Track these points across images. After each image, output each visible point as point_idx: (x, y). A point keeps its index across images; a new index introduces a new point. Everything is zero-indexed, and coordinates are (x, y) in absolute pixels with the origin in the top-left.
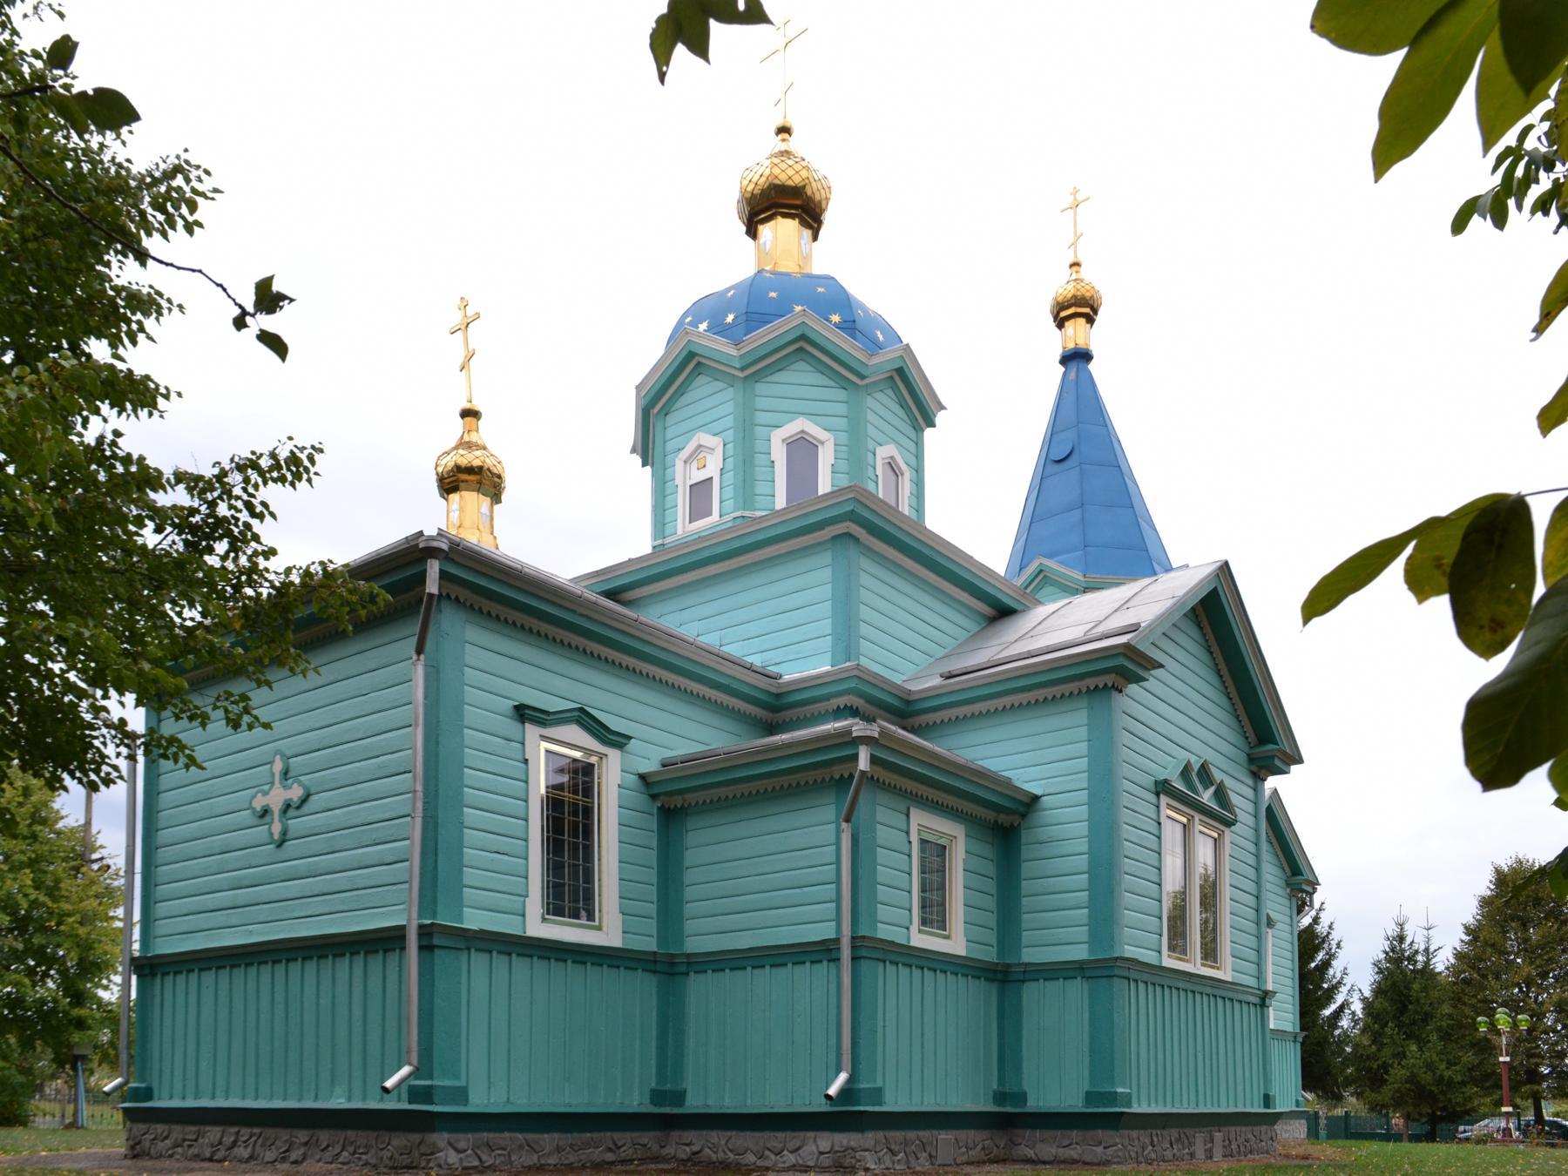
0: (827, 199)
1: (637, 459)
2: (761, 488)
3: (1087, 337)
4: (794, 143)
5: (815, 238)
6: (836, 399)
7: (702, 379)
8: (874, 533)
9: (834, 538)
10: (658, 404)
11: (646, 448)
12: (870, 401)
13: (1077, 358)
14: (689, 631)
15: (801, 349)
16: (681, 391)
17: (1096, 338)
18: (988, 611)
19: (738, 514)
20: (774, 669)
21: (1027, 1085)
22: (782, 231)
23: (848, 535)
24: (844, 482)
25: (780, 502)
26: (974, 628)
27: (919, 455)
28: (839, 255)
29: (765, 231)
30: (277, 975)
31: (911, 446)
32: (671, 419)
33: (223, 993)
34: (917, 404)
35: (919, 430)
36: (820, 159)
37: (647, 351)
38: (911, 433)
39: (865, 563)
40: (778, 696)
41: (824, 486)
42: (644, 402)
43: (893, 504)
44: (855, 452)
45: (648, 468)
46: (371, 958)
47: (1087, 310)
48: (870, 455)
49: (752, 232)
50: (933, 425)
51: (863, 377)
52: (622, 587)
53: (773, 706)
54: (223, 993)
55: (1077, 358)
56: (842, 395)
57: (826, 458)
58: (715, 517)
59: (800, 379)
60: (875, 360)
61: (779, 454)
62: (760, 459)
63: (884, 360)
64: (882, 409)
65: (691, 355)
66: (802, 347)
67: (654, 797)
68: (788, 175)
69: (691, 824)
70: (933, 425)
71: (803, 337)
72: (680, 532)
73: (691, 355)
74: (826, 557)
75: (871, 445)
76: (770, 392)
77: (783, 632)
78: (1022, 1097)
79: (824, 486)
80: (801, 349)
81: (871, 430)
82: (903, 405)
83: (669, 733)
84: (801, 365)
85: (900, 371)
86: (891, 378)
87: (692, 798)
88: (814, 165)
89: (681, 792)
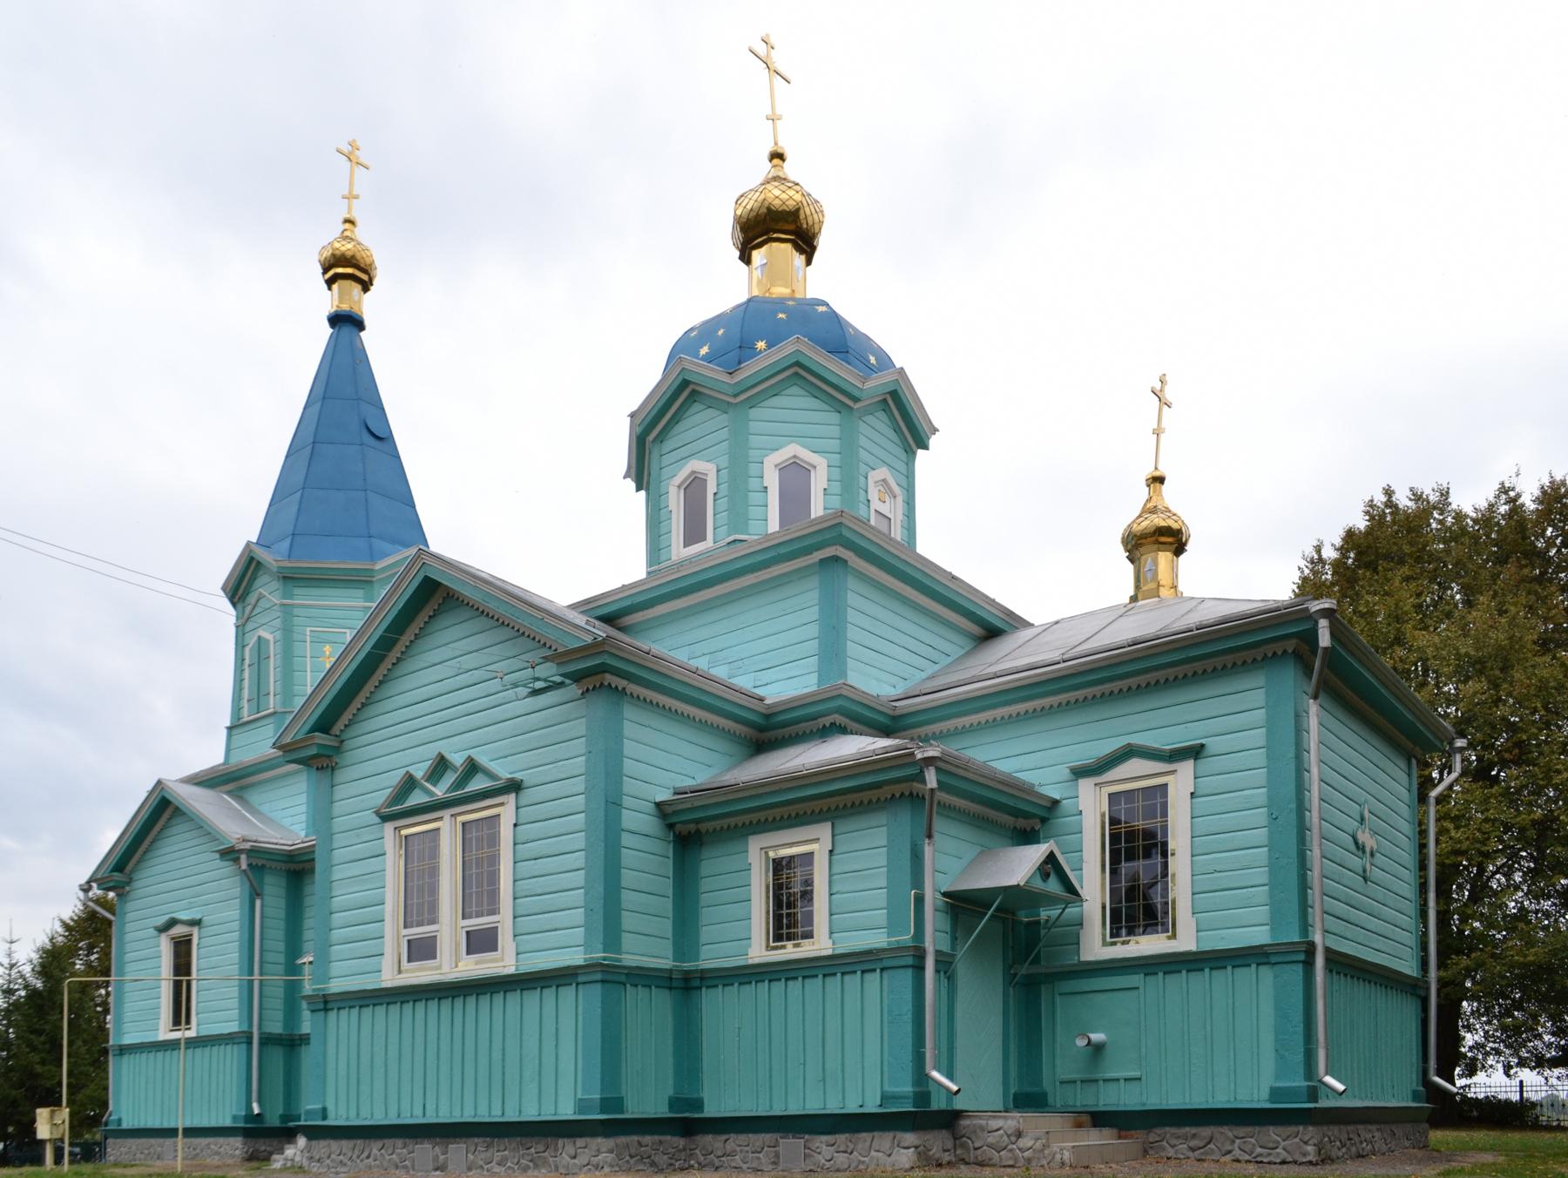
0: (821, 223)
1: (631, 484)
2: (754, 512)
3: (360, 301)
4: (790, 169)
5: (809, 262)
6: (827, 421)
7: (697, 407)
8: (854, 556)
9: (821, 561)
10: (653, 434)
11: (641, 470)
12: (863, 427)
13: (346, 322)
14: (681, 656)
15: (796, 374)
16: (676, 419)
17: (369, 306)
18: (977, 630)
19: (731, 538)
20: (759, 692)
21: (706, 1095)
22: (780, 252)
23: (835, 559)
24: (836, 503)
25: (774, 525)
26: (969, 645)
27: (910, 476)
28: (833, 279)
29: (758, 256)
30: (443, 1013)
31: (903, 468)
32: (669, 445)
33: (394, 1029)
34: (912, 431)
35: (911, 454)
36: (815, 180)
37: (642, 377)
38: (903, 456)
39: (852, 583)
40: (767, 716)
41: (817, 509)
42: (638, 430)
43: (885, 531)
44: (849, 479)
45: (643, 493)
46: (546, 991)
47: (365, 277)
48: (862, 479)
49: (746, 258)
50: (926, 447)
51: (856, 400)
52: (614, 613)
53: (766, 730)
54: (366, 1032)
55: (346, 322)
56: (834, 417)
57: (819, 481)
58: (709, 543)
59: (795, 403)
60: (869, 385)
61: (772, 480)
62: (753, 483)
63: (876, 384)
64: (875, 432)
65: (685, 383)
66: (799, 373)
67: (671, 826)
68: (778, 196)
69: (706, 852)
70: (926, 447)
71: (798, 364)
72: (674, 558)
73: (685, 383)
74: (814, 582)
75: (863, 468)
76: (762, 417)
77: (763, 654)
78: (698, 1104)
79: (817, 509)
80: (796, 374)
81: (863, 454)
82: (897, 430)
83: (673, 761)
84: (795, 390)
85: (894, 394)
86: (885, 400)
87: (709, 826)
88: (808, 188)
89: (698, 821)
